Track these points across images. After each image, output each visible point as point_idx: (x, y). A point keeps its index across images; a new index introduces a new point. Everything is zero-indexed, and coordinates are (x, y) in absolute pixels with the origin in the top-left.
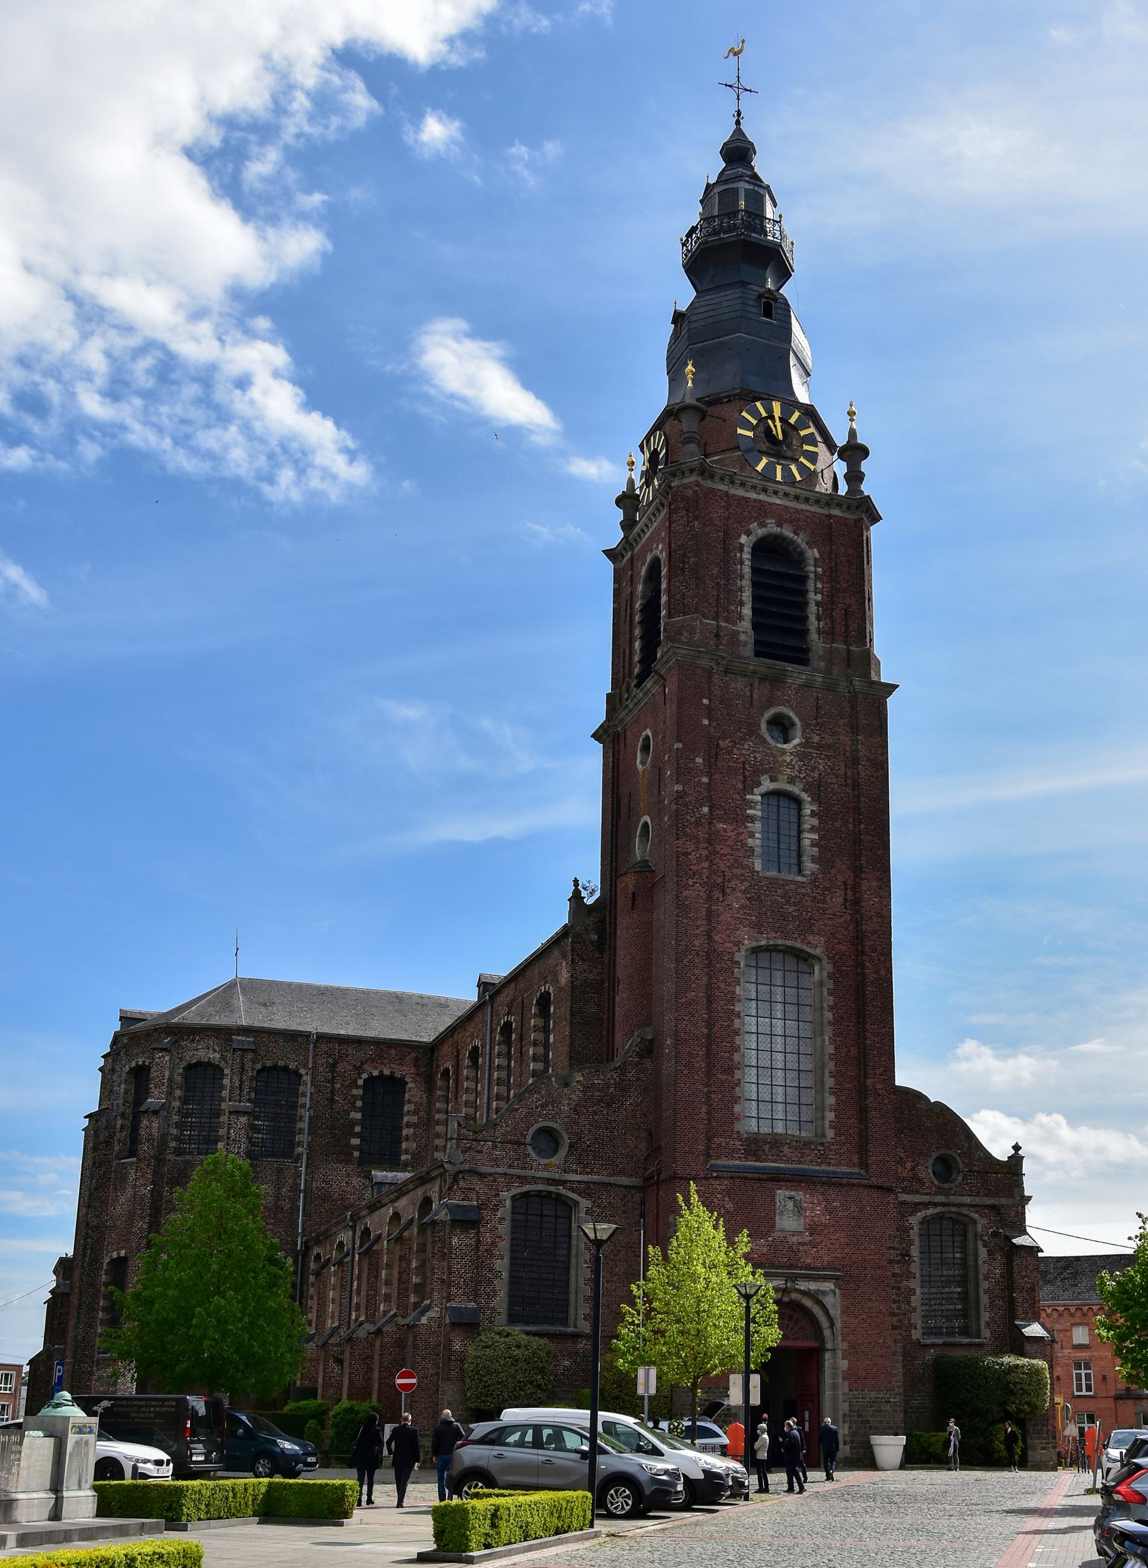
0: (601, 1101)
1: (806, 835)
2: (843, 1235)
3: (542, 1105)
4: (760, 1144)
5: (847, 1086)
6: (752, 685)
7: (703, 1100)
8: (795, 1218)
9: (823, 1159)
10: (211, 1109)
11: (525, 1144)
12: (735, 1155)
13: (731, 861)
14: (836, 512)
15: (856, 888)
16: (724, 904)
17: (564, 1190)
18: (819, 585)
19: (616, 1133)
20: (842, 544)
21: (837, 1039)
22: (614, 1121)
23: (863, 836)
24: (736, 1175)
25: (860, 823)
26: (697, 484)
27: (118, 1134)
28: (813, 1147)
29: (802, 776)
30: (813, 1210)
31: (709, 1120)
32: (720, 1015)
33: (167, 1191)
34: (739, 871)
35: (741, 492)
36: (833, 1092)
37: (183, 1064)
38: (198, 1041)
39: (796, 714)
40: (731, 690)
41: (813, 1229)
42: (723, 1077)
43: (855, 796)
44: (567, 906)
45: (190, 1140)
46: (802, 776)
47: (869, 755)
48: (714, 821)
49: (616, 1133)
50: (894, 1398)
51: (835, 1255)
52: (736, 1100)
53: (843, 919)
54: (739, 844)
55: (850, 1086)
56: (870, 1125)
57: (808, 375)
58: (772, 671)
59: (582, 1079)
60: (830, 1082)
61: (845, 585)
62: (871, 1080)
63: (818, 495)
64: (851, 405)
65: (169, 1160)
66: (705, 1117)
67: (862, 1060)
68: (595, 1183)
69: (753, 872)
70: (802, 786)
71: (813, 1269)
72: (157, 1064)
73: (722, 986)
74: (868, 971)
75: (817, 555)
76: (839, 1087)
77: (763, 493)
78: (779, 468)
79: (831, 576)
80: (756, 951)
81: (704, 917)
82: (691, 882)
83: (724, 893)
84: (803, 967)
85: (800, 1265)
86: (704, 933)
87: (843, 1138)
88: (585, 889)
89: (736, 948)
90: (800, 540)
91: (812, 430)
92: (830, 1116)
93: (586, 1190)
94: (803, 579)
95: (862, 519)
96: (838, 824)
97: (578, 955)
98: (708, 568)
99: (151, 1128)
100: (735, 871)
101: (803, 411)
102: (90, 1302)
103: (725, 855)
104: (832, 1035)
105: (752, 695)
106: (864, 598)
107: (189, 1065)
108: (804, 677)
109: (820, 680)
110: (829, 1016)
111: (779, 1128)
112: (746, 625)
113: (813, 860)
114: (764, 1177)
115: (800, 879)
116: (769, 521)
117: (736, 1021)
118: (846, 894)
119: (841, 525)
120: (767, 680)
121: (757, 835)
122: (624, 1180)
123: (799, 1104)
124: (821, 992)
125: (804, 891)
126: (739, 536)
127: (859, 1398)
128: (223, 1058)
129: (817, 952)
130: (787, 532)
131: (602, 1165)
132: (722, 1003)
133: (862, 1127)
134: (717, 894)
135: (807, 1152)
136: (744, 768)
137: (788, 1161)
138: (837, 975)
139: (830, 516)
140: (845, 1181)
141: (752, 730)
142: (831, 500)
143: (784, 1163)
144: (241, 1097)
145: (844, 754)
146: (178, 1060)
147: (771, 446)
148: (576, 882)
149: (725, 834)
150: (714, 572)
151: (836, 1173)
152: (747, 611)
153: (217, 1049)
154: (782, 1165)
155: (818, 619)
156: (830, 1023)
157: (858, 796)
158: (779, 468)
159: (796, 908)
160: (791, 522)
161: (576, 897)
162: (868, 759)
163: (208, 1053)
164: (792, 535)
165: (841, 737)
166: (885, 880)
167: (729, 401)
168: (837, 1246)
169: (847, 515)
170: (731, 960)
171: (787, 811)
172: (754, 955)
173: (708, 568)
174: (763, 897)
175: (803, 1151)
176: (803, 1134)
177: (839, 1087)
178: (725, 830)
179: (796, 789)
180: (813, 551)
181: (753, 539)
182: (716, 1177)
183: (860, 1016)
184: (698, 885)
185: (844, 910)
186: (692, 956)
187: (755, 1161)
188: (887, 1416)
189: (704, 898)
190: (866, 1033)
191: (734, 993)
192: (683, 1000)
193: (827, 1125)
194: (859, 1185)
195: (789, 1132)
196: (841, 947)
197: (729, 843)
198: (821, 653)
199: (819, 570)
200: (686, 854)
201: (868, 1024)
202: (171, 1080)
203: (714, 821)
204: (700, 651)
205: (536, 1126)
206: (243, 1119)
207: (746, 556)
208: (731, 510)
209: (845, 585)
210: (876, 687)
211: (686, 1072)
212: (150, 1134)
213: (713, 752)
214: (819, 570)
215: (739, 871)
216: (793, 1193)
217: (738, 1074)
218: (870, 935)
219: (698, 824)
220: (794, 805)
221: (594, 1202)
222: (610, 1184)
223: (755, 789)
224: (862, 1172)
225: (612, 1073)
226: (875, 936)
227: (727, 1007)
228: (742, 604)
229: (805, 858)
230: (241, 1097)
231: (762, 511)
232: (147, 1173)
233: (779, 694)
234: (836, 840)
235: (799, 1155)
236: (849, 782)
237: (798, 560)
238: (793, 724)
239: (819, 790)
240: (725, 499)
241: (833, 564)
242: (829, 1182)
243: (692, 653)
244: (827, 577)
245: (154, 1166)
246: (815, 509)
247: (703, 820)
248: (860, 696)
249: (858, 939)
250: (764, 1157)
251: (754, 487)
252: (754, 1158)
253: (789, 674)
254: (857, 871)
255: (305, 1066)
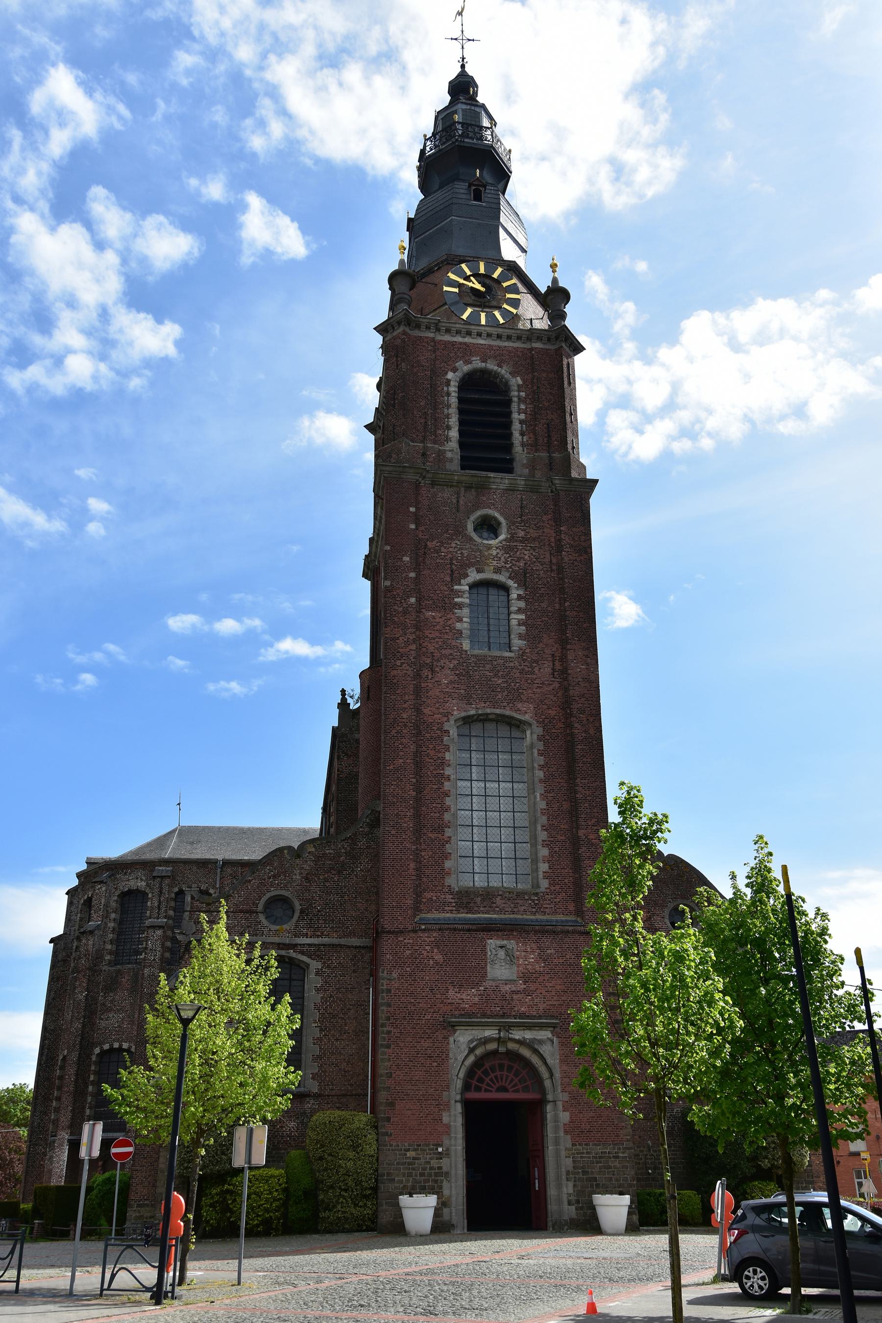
0: (333, 868)
1: (513, 616)
2: (559, 982)
3: (274, 876)
4: (472, 896)
5: (560, 838)
6: (458, 494)
7: (411, 857)
8: (508, 966)
9: (538, 908)
10: (140, 927)
11: (257, 913)
12: (446, 908)
13: (440, 643)
14: (538, 345)
15: (563, 659)
16: (433, 681)
17: (295, 954)
18: (523, 407)
19: (346, 898)
20: (543, 370)
21: (549, 795)
22: (345, 887)
23: (568, 612)
24: (444, 927)
25: (565, 601)
26: (404, 333)
27: (74, 954)
28: (526, 898)
29: (508, 566)
30: (526, 958)
31: (417, 875)
32: (430, 779)
33: (102, 996)
34: (447, 652)
35: (447, 338)
36: (545, 844)
37: (118, 893)
38: (130, 873)
39: (501, 514)
40: (437, 499)
41: (527, 977)
42: (433, 836)
43: (560, 579)
44: (337, 711)
45: (123, 953)
46: (508, 566)
47: (572, 542)
48: (423, 610)
49: (346, 898)
50: (623, 1153)
51: (550, 1003)
52: (447, 856)
53: (551, 687)
54: (448, 628)
55: (563, 838)
56: (584, 873)
57: (526, 252)
58: (475, 479)
59: (313, 850)
60: (542, 835)
61: (547, 404)
62: (583, 831)
63: (519, 332)
64: (553, 259)
65: (105, 971)
66: (414, 873)
67: (574, 813)
68: (324, 945)
69: (461, 651)
70: (508, 575)
71: (528, 1017)
72: (97, 894)
73: (432, 753)
74: (577, 731)
75: (520, 382)
76: (552, 839)
77: (468, 336)
78: (483, 315)
79: (534, 397)
80: (467, 721)
81: (412, 693)
82: (398, 663)
83: (433, 671)
84: (516, 733)
85: (514, 1013)
86: (412, 707)
87: (557, 887)
88: (352, 697)
89: (446, 719)
90: (504, 371)
91: (514, 281)
92: (544, 867)
93: (316, 952)
94: (508, 403)
95: (562, 347)
96: (544, 605)
97: (343, 752)
98: (415, 401)
99: (87, 945)
100: (443, 652)
101: (506, 268)
102: (46, 1094)
103: (434, 639)
104: (543, 792)
105: (458, 501)
106: (564, 412)
107: (122, 893)
108: (507, 481)
109: (523, 483)
110: (540, 774)
111: (495, 882)
112: (454, 444)
113: (521, 636)
114: (474, 927)
115: (508, 654)
116: (474, 358)
117: (446, 784)
118: (554, 664)
119: (543, 355)
120: (472, 488)
121: (465, 619)
122: (355, 941)
123: (515, 859)
124: (532, 753)
125: (512, 664)
126: (446, 373)
127: (583, 1153)
128: (148, 885)
129: (527, 717)
130: (491, 366)
131: (332, 928)
132: (432, 768)
133: (576, 876)
134: (426, 672)
135: (521, 902)
136: (451, 564)
137: (501, 911)
138: (547, 737)
139: (531, 349)
140: (559, 928)
141: (459, 531)
142: (533, 334)
143: (497, 914)
144: (159, 914)
145: (549, 545)
146: (114, 890)
147: (477, 299)
148: (343, 692)
149: (434, 620)
150: (421, 404)
151: (551, 921)
152: (454, 433)
153: (144, 878)
154: (495, 916)
155: (522, 434)
156: (541, 781)
157: (562, 579)
158: (483, 315)
159: (504, 680)
160: (495, 357)
161: (343, 705)
162: (571, 546)
163: (135, 881)
164: (496, 368)
165: (545, 530)
166: (591, 649)
167: (439, 268)
168: (553, 994)
169: (548, 347)
170: (441, 729)
171: (494, 595)
172: (468, 726)
173: (415, 401)
174: (471, 673)
175: (516, 901)
176: (519, 886)
177: (552, 839)
178: (434, 617)
179: (502, 578)
180: (516, 380)
181: (459, 374)
182: (425, 930)
183: (571, 773)
184: (406, 665)
185: (553, 679)
186: (399, 728)
187: (467, 913)
188: (616, 1173)
189: (412, 675)
190: (576, 788)
191: (444, 758)
192: (391, 767)
193: (541, 876)
194: (574, 932)
195: (505, 885)
196: (550, 712)
197: (438, 627)
198: (525, 462)
199: (523, 394)
200: (395, 639)
201: (579, 779)
202: (106, 905)
203: (423, 610)
204: (405, 467)
205: (268, 895)
206: (159, 932)
207: (453, 389)
208: (438, 353)
209: (547, 404)
210: (576, 483)
211: (393, 832)
212: (87, 950)
213: (422, 551)
214: (523, 394)
215: (447, 652)
216: (505, 942)
217: (448, 832)
218: (578, 698)
219: (405, 612)
220: (502, 593)
221: (324, 963)
222: (340, 946)
223: (462, 581)
224: (579, 919)
225: (343, 843)
226: (583, 699)
227: (437, 772)
228: (449, 428)
229: (512, 636)
230: (159, 914)
231: (467, 351)
232: (83, 982)
233: (484, 499)
234: (543, 619)
235: (512, 905)
236: (554, 567)
237: (505, 389)
238: (499, 524)
239: (525, 577)
240: (432, 344)
241: (535, 388)
242: (543, 930)
243: (397, 469)
244: (530, 399)
245: (89, 976)
246: (518, 345)
247: (410, 609)
248: (561, 493)
249: (566, 704)
250: (476, 909)
251: (458, 332)
252: (466, 911)
253: (492, 480)
254: (563, 643)
255: (214, 887)
